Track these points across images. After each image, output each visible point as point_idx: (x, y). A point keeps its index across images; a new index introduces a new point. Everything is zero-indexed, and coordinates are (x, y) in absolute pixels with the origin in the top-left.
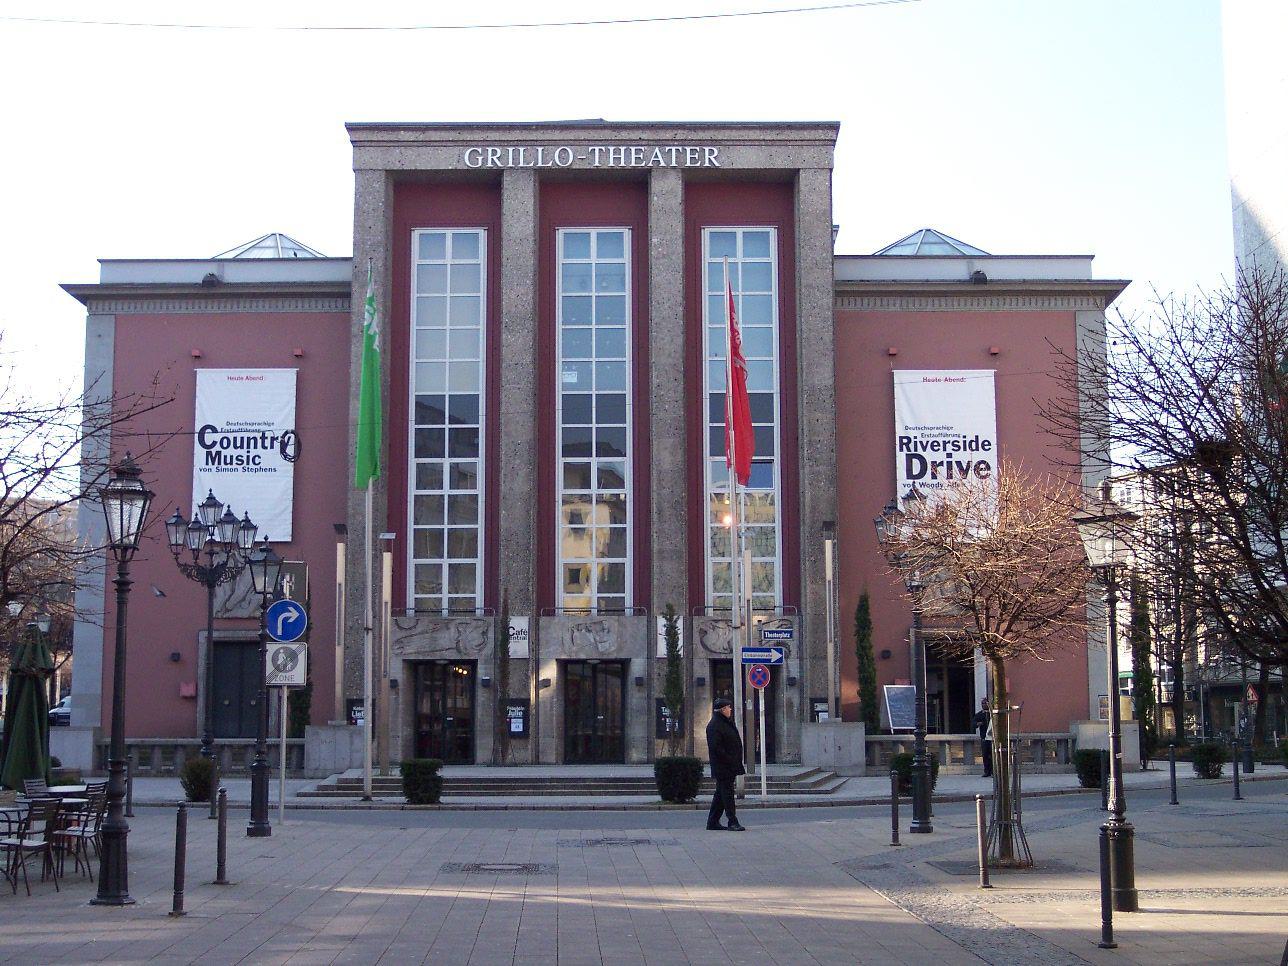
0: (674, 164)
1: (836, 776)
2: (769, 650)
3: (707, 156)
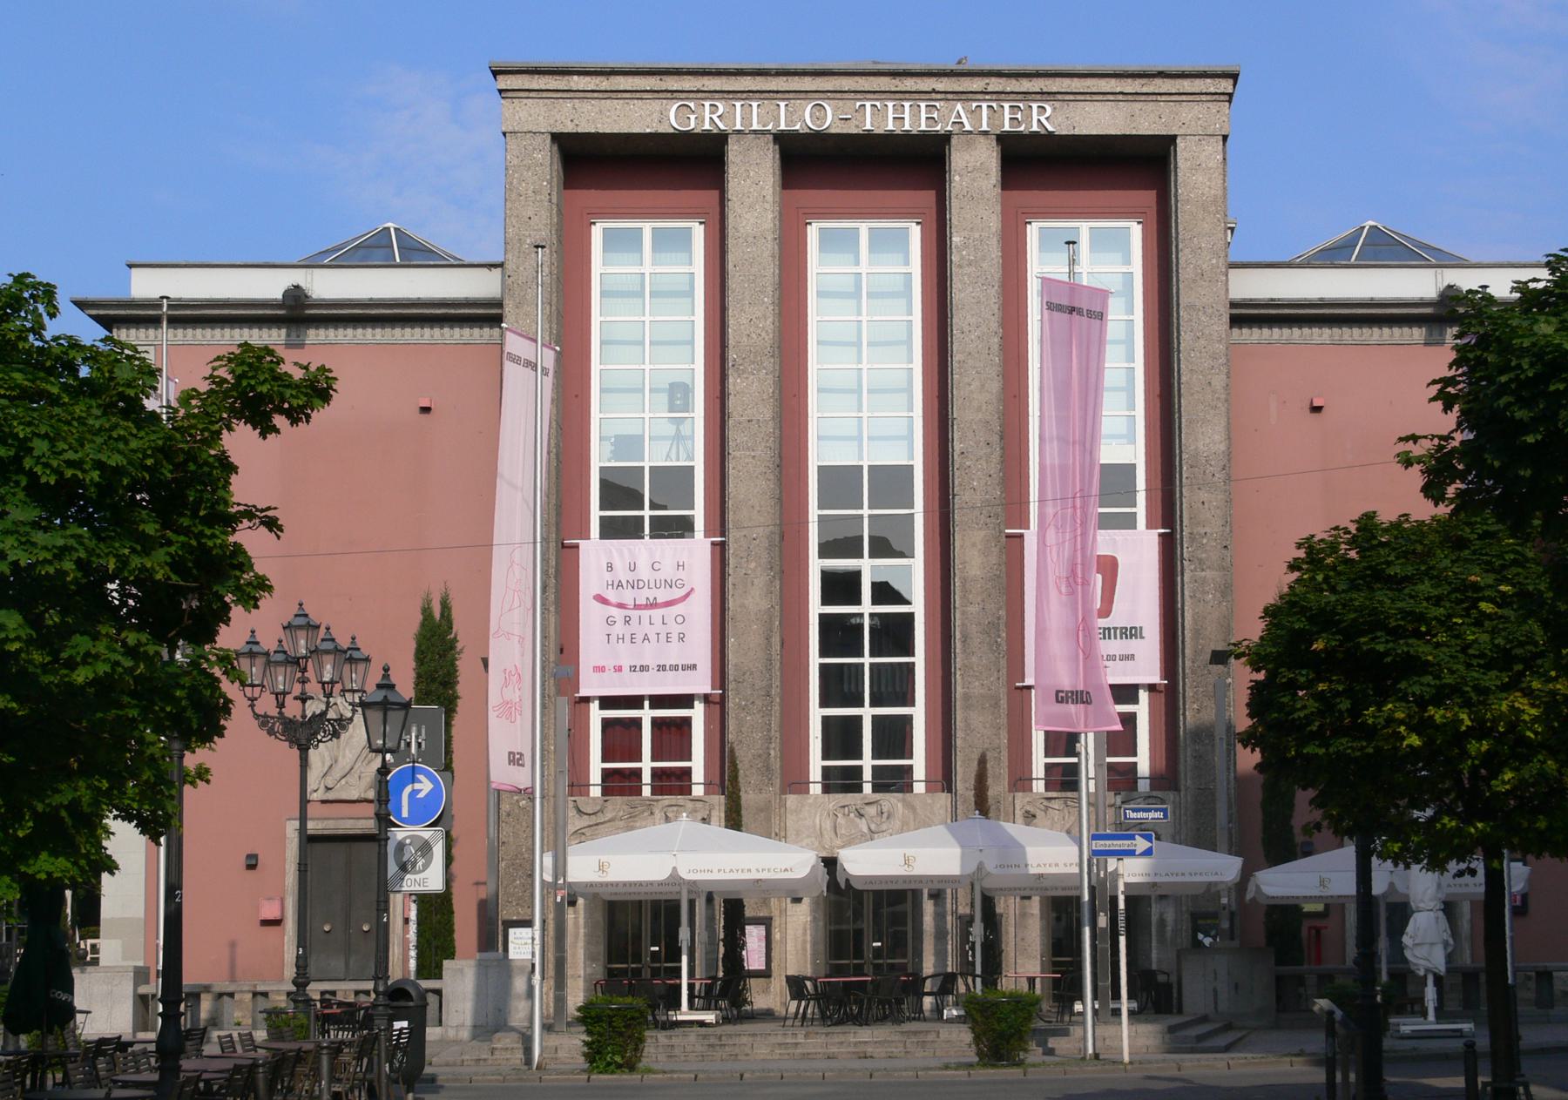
0: (985, 128)
1: (1228, 1027)
3: (1035, 117)
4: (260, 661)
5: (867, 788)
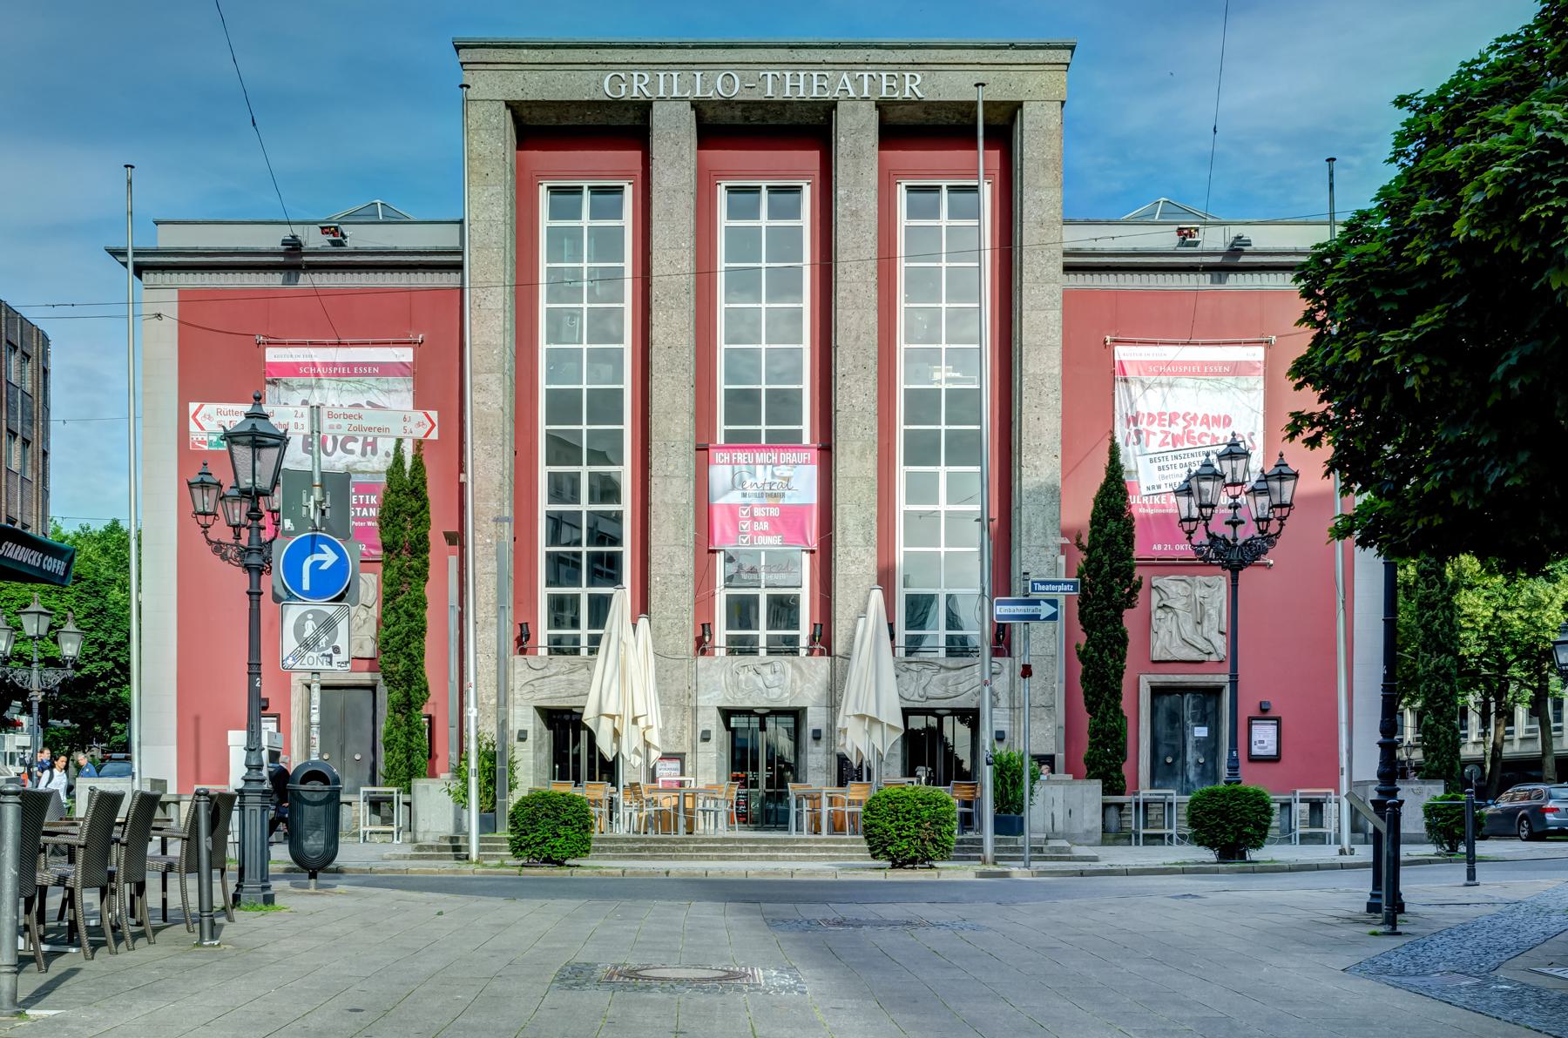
0: (866, 94)
2: (1037, 602)
4: (213, 493)
5: (763, 652)
